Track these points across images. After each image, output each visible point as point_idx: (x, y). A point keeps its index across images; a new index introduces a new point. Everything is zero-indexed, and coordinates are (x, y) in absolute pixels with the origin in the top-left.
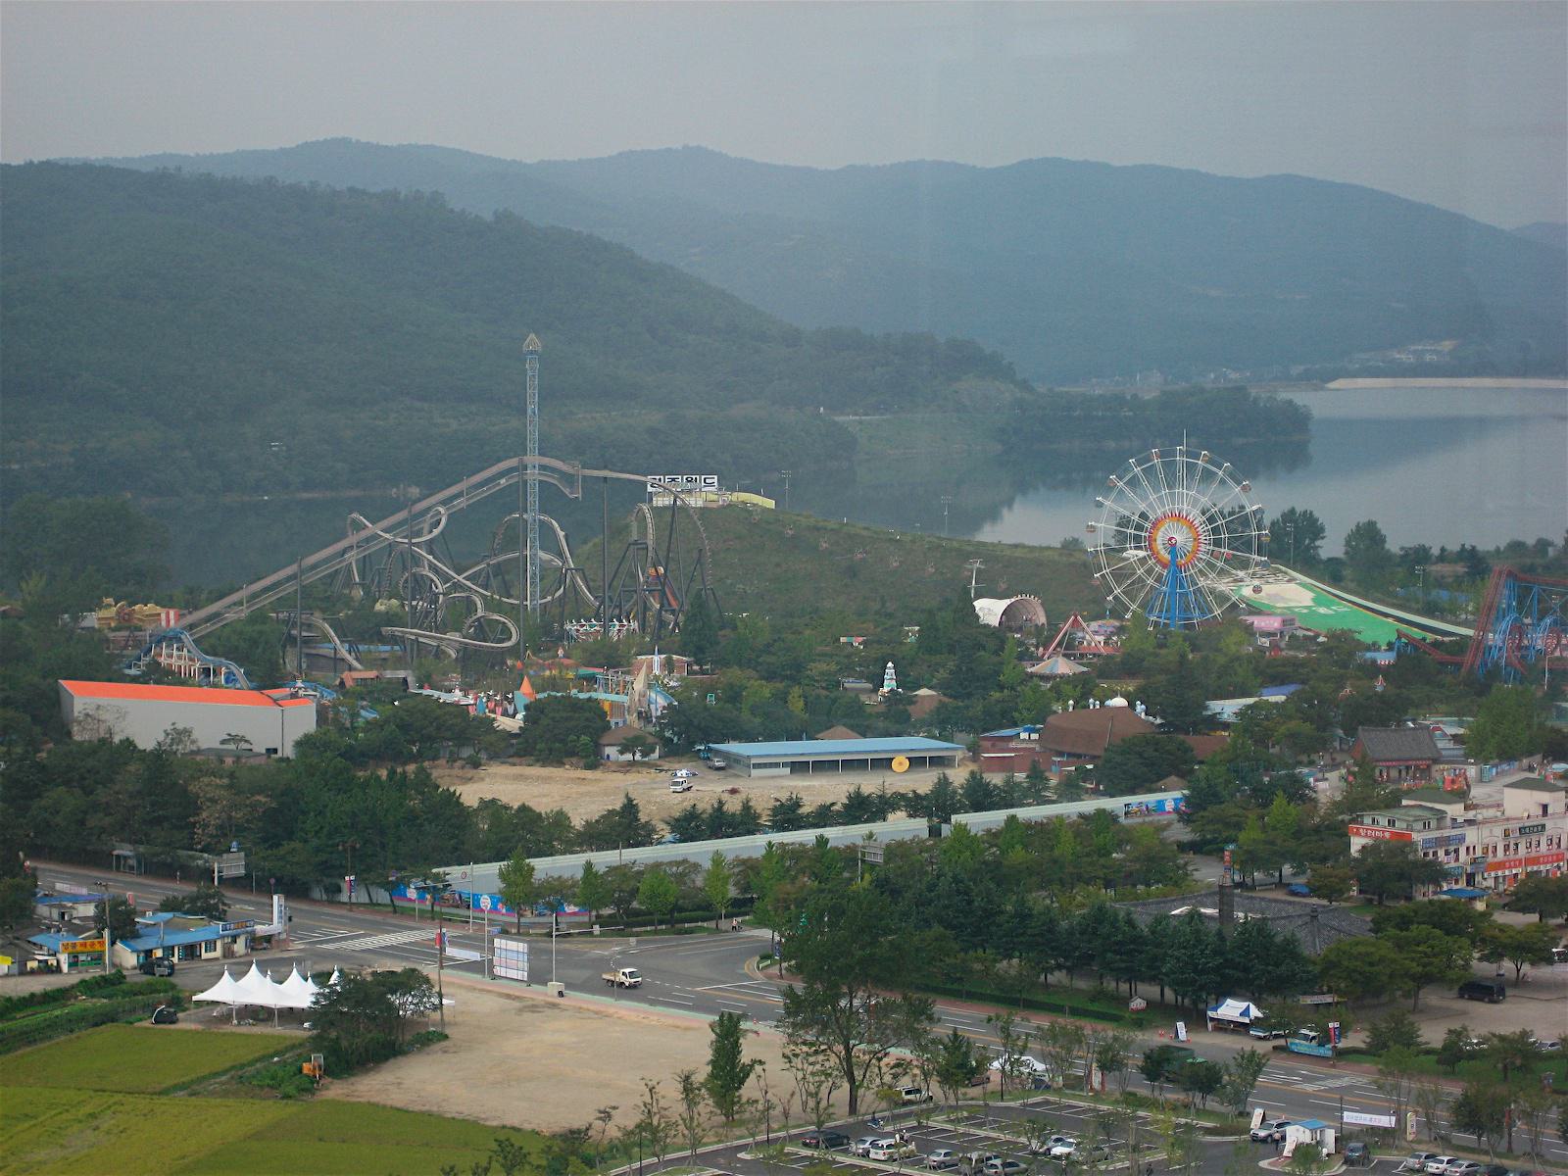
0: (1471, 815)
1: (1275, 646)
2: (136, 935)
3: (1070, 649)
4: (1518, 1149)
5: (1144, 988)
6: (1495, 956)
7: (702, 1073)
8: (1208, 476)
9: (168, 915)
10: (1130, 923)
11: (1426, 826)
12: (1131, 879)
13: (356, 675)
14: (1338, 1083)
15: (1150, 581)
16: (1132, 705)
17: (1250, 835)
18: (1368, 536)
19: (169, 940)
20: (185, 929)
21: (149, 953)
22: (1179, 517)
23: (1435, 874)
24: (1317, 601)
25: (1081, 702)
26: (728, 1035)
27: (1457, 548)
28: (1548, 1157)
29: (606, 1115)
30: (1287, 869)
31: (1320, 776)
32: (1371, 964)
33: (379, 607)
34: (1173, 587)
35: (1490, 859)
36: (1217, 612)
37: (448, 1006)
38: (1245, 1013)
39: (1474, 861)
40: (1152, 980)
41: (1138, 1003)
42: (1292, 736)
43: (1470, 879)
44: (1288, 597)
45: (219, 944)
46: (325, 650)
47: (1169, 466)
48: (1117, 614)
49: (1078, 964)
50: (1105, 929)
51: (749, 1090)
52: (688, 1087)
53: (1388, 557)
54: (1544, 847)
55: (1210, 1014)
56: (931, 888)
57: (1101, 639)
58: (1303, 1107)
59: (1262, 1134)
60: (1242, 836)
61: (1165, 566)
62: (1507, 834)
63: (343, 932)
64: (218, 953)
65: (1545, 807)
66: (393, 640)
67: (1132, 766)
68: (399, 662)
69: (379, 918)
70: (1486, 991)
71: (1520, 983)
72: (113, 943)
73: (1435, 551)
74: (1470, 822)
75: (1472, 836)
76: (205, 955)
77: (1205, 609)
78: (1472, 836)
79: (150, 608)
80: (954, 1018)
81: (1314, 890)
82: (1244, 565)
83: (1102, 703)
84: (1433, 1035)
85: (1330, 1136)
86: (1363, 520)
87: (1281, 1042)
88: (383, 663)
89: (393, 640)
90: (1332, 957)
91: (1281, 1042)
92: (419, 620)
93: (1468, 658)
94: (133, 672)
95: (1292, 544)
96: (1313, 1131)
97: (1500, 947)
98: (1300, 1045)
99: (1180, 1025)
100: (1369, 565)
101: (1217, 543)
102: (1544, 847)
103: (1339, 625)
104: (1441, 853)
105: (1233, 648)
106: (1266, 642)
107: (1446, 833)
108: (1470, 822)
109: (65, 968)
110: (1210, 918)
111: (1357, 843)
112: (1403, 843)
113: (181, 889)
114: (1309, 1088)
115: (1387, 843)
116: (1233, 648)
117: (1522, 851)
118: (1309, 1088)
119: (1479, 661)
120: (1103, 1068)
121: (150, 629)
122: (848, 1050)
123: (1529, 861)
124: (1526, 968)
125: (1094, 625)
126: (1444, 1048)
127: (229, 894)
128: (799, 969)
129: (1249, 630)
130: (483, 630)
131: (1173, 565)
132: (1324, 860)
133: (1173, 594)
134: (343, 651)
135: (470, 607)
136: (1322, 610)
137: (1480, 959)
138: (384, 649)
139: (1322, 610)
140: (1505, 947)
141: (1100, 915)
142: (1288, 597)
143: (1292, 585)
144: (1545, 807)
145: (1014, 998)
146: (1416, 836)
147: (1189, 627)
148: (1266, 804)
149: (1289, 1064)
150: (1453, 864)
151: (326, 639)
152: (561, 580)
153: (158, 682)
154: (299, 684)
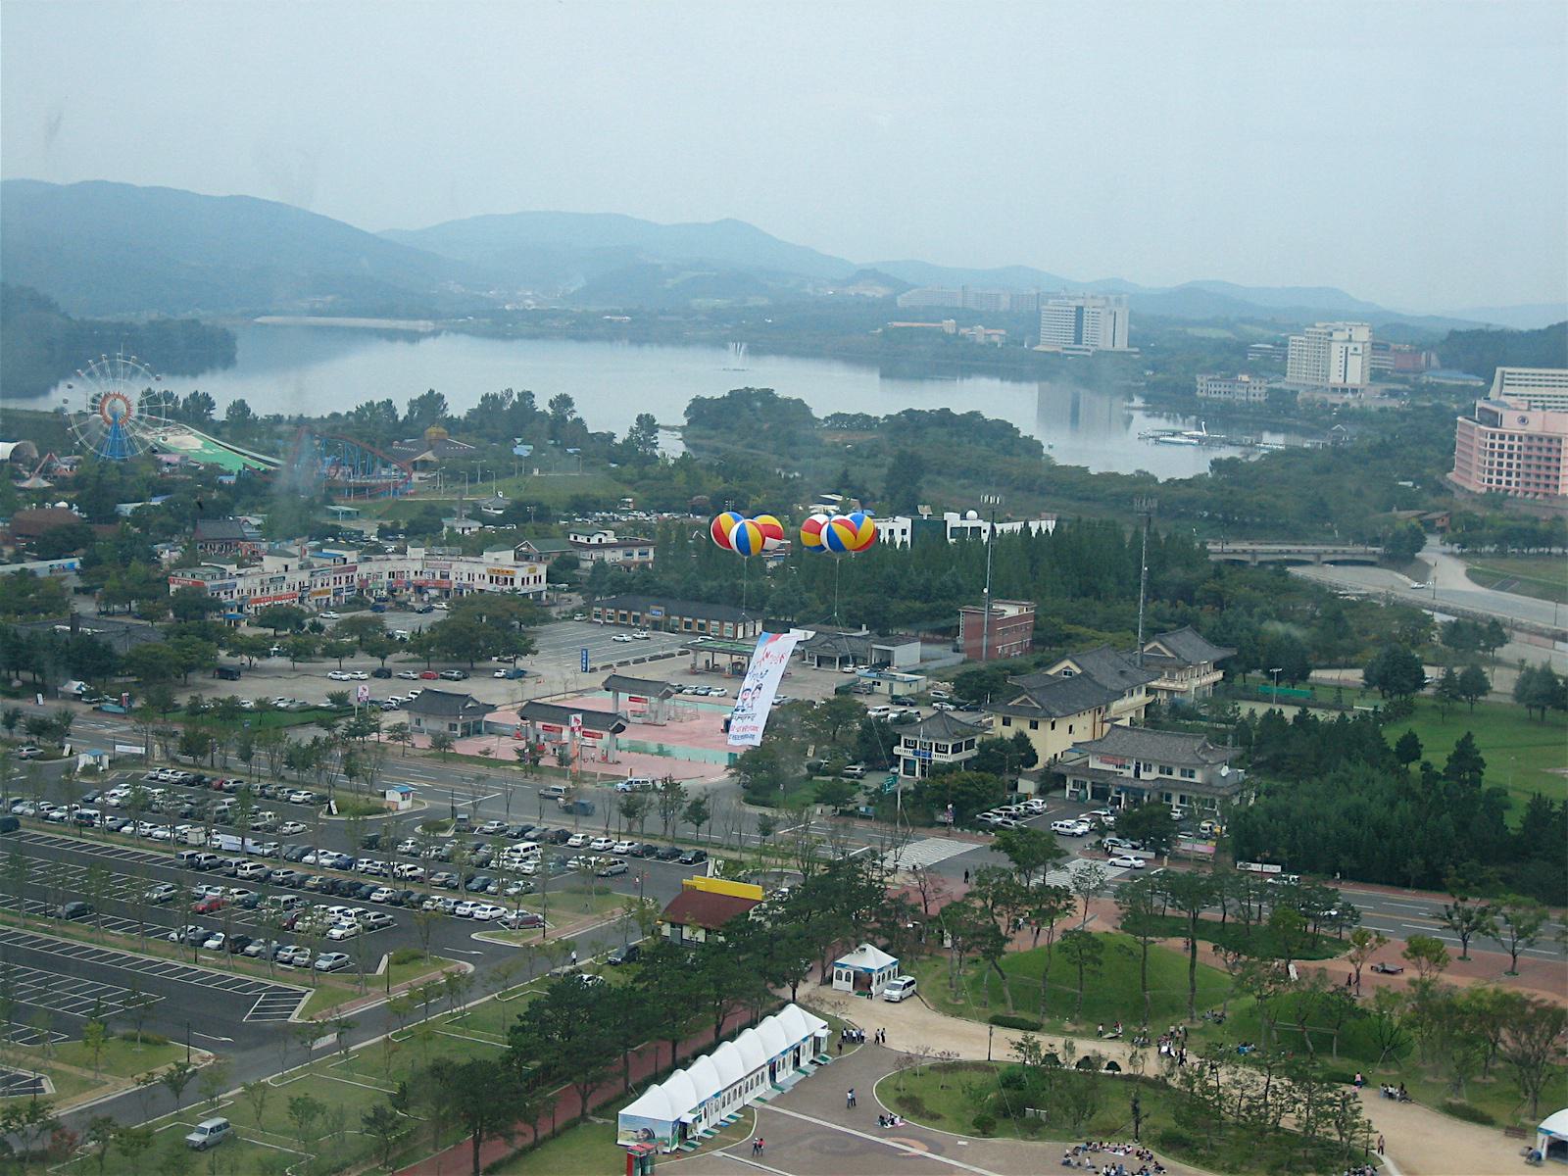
1: (173, 472)
3: (46, 472)
4: (217, 764)
5: (24, 675)
8: (136, 371)
10: (16, 636)
11: (214, 577)
12: (36, 610)
16: (71, 507)
17: (112, 583)
18: (240, 409)
22: (125, 400)
24: (204, 446)
25: (40, 505)
28: (233, 769)
31: (172, 548)
32: (156, 658)
34: (115, 436)
35: (252, 596)
36: (141, 452)
37: (601, 824)
38: (79, 689)
39: (242, 598)
41: (16, 683)
42: (162, 525)
43: (240, 609)
44: (189, 443)
47: (112, 365)
55: (59, 689)
57: (68, 467)
59: (1310, 920)
60: (108, 583)
61: (109, 423)
62: (262, 583)
65: (286, 567)
67: (52, 544)
71: (251, 669)
77: (134, 450)
78: (240, 583)
82: (158, 423)
83: (53, 505)
85: (106, 759)
87: (97, 705)
90: (134, 655)
91: (97, 705)
95: (196, 413)
96: (95, 757)
97: (238, 649)
98: (109, 707)
99: (40, 696)
103: (215, 460)
104: (222, 594)
105: (145, 473)
106: (166, 469)
107: (225, 581)
108: (240, 575)
111: (173, 588)
112: (199, 588)
114: (108, 731)
115: (189, 587)
116: (145, 473)
117: (272, 592)
123: (276, 598)
124: (255, 660)
125: (64, 459)
129: (159, 464)
131: (115, 424)
133: (114, 441)
136: (207, 451)
139: (207, 451)
140: (242, 647)
142: (189, 443)
143: (191, 436)
144: (286, 567)
146: (206, 584)
149: (100, 717)
150: (229, 600)
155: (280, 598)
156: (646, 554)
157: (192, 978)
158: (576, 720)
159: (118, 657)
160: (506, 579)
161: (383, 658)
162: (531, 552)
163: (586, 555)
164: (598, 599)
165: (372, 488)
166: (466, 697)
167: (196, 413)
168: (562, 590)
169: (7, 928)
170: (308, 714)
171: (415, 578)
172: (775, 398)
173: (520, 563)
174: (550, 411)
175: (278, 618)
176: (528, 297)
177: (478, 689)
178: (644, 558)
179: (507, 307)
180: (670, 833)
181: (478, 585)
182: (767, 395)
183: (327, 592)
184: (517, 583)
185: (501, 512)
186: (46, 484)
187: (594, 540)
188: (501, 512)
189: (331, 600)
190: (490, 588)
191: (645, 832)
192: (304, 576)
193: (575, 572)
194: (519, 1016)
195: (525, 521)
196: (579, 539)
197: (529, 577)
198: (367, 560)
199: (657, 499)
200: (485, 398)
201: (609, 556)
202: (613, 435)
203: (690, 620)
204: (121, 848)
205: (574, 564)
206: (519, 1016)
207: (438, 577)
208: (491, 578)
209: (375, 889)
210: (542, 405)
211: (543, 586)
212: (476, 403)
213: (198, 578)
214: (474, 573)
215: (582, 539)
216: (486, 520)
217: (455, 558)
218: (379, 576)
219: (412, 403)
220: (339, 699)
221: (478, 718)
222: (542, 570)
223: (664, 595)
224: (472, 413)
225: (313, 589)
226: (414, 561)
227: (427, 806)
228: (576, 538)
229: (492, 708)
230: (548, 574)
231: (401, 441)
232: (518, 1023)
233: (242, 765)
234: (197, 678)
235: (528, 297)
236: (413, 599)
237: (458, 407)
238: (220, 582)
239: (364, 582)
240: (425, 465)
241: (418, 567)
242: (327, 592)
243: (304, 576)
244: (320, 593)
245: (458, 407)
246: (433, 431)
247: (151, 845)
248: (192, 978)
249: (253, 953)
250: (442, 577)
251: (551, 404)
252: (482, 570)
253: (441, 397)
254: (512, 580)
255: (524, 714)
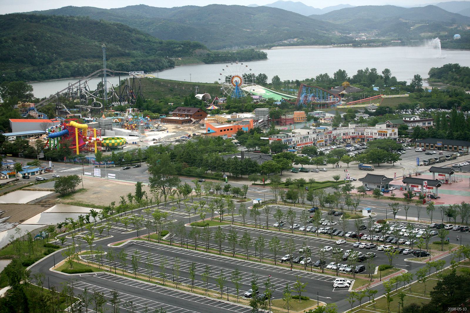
0: (293, 135)
2: (22, 170)
3: (216, 104)
6: (297, 164)
7: (134, 194)
9: (28, 166)
10: (223, 160)
11: (284, 137)
13: (69, 115)
14: (265, 191)
15: (232, 89)
18: (276, 79)
19: (28, 172)
20: (32, 169)
21: (25, 174)
22: (237, 76)
23: (287, 147)
26: (139, 186)
27: (295, 81)
29: (113, 204)
30: (257, 148)
33: (75, 101)
39: (294, 144)
40: (228, 171)
43: (294, 148)
45: (39, 172)
46: (64, 110)
48: (226, 96)
49: (213, 169)
50: (218, 162)
51: (144, 198)
52: (130, 196)
53: (281, 83)
54: (308, 141)
56: (183, 155)
58: (256, 195)
61: (235, 86)
63: (64, 168)
64: (39, 173)
65: (308, 133)
66: (77, 108)
68: (79, 112)
69: (72, 165)
70: (295, 171)
72: (17, 172)
73: (291, 81)
74: (293, 136)
75: (294, 139)
76: (36, 174)
78: (294, 139)
79: (28, 103)
80: (185, 181)
81: (262, 152)
84: (284, 180)
86: (275, 75)
88: (75, 112)
89: (77, 108)
92: (82, 103)
93: (296, 102)
94: (25, 116)
95: (261, 80)
100: (277, 84)
101: (245, 81)
102: (308, 141)
107: (288, 139)
108: (293, 136)
109: (8, 178)
110: (239, 158)
112: (280, 140)
113: (31, 161)
114: (259, 192)
117: (304, 141)
118: (259, 192)
119: (298, 103)
120: (217, 190)
121: (28, 107)
122: (164, 189)
123: (306, 144)
126: (286, 182)
127: (41, 161)
128: (152, 173)
129: (253, 99)
130: (96, 105)
132: (264, 145)
134: (67, 111)
135: (93, 100)
136: (267, 94)
137: (294, 164)
138: (75, 109)
139: (267, 94)
141: (217, 159)
144: (308, 133)
145: (201, 176)
147: (240, 98)
148: (253, 134)
151: (64, 108)
152: (112, 94)
153: (30, 118)
154: (57, 117)
155: (307, 144)
156: (430, 123)
157: (311, 277)
158: (425, 183)
159: (259, 167)
160: (384, 134)
161: (348, 163)
162: (390, 124)
163: (409, 125)
164: (417, 140)
165: (327, 104)
166: (383, 176)
167: (261, 80)
168: (403, 137)
169: (243, 260)
170: (326, 184)
171: (352, 135)
172: (459, 67)
173: (388, 128)
174: (383, 75)
175: (311, 151)
176: (363, 36)
177: (388, 173)
178: (429, 125)
179: (357, 39)
180: (464, 222)
181: (374, 136)
182: (456, 66)
183: (322, 141)
184: (388, 135)
185: (375, 111)
186: (216, 108)
187: (412, 119)
188: (375, 111)
189: (324, 144)
190: (379, 137)
191: (456, 222)
192: (315, 136)
193: (407, 131)
194: (434, 288)
195: (381, 114)
196: (407, 119)
197: (392, 133)
198: (335, 129)
199: (428, 104)
200: (359, 71)
201: (417, 124)
202: (405, 83)
203: (451, 146)
204: (239, 226)
205: (406, 128)
206: (434, 288)
207: (360, 134)
208: (379, 134)
209: (404, 250)
210: (380, 73)
211: (397, 136)
212: (356, 73)
213: (279, 138)
214: (373, 132)
215: (408, 119)
216: (371, 114)
217: (365, 127)
218: (339, 135)
219: (335, 74)
220: (337, 178)
221: (387, 183)
222: (396, 130)
223: (441, 138)
224: (355, 77)
225: (318, 140)
226: (351, 129)
227: (376, 215)
228: (405, 119)
229: (392, 179)
230: (399, 132)
231: (334, 87)
232: (433, 290)
233: (309, 202)
234: (285, 173)
235: (363, 36)
236: (352, 142)
237: (351, 74)
238: (287, 139)
239: (335, 137)
240: (343, 95)
241: (353, 131)
242: (322, 141)
243: (315, 136)
244: (320, 141)
245: (351, 74)
246: (345, 83)
247: (285, 231)
248: (311, 277)
249: (330, 268)
250: (361, 134)
251: (383, 73)
252: (376, 131)
253: (344, 71)
254: (386, 134)
255: (405, 181)
